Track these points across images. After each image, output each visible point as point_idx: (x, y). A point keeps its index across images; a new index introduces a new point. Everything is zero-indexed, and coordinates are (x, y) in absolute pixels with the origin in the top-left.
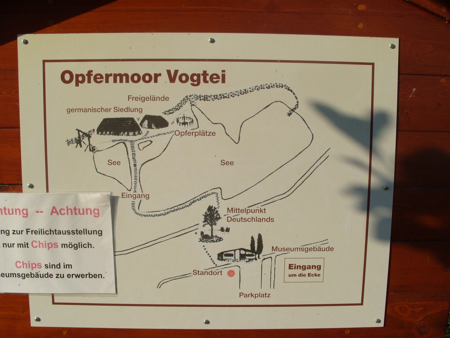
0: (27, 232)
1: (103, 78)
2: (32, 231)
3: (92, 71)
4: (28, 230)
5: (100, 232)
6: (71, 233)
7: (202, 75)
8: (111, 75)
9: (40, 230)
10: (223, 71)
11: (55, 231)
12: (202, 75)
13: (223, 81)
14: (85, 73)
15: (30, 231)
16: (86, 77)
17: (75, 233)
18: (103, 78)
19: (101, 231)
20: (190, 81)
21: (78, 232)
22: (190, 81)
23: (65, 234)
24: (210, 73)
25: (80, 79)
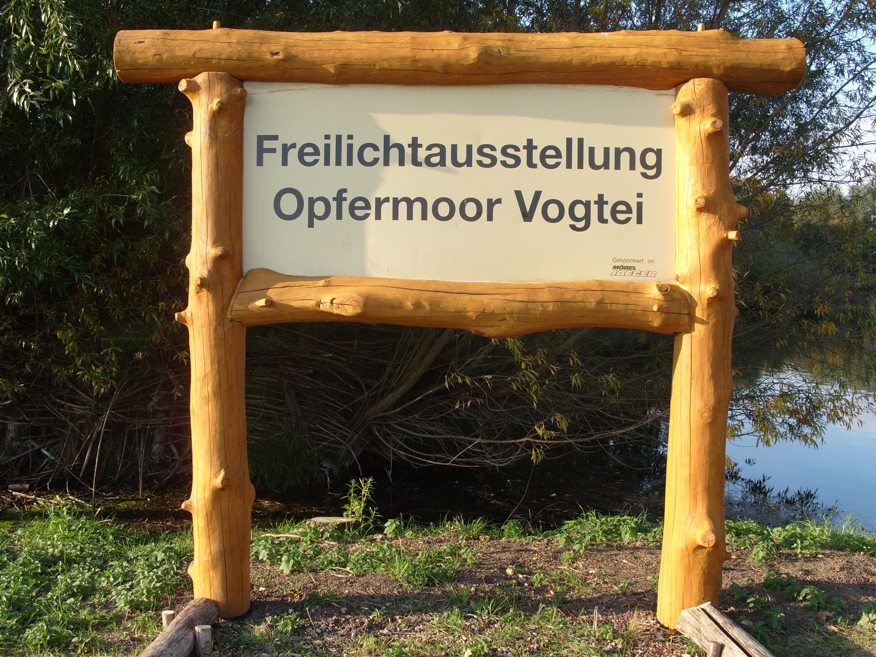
0: (261, 151)
1: (370, 208)
2: (286, 149)
3: (345, 191)
4: (267, 144)
5: (651, 159)
6: (500, 157)
7: (595, 203)
8: (387, 200)
9: (333, 142)
10: (640, 195)
11: (415, 144)
12: (595, 203)
13: (639, 221)
14: (330, 195)
15: (277, 145)
16: (334, 205)
17: (518, 161)
18: (370, 208)
19: (658, 153)
20: (567, 220)
21: (536, 154)
22: (567, 220)
23: (469, 163)
24: (611, 199)
25: (319, 208)
